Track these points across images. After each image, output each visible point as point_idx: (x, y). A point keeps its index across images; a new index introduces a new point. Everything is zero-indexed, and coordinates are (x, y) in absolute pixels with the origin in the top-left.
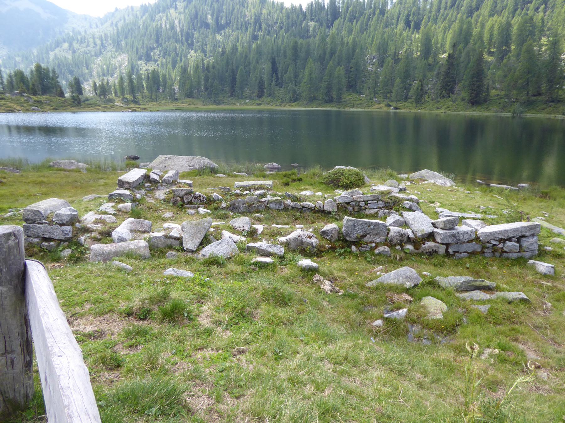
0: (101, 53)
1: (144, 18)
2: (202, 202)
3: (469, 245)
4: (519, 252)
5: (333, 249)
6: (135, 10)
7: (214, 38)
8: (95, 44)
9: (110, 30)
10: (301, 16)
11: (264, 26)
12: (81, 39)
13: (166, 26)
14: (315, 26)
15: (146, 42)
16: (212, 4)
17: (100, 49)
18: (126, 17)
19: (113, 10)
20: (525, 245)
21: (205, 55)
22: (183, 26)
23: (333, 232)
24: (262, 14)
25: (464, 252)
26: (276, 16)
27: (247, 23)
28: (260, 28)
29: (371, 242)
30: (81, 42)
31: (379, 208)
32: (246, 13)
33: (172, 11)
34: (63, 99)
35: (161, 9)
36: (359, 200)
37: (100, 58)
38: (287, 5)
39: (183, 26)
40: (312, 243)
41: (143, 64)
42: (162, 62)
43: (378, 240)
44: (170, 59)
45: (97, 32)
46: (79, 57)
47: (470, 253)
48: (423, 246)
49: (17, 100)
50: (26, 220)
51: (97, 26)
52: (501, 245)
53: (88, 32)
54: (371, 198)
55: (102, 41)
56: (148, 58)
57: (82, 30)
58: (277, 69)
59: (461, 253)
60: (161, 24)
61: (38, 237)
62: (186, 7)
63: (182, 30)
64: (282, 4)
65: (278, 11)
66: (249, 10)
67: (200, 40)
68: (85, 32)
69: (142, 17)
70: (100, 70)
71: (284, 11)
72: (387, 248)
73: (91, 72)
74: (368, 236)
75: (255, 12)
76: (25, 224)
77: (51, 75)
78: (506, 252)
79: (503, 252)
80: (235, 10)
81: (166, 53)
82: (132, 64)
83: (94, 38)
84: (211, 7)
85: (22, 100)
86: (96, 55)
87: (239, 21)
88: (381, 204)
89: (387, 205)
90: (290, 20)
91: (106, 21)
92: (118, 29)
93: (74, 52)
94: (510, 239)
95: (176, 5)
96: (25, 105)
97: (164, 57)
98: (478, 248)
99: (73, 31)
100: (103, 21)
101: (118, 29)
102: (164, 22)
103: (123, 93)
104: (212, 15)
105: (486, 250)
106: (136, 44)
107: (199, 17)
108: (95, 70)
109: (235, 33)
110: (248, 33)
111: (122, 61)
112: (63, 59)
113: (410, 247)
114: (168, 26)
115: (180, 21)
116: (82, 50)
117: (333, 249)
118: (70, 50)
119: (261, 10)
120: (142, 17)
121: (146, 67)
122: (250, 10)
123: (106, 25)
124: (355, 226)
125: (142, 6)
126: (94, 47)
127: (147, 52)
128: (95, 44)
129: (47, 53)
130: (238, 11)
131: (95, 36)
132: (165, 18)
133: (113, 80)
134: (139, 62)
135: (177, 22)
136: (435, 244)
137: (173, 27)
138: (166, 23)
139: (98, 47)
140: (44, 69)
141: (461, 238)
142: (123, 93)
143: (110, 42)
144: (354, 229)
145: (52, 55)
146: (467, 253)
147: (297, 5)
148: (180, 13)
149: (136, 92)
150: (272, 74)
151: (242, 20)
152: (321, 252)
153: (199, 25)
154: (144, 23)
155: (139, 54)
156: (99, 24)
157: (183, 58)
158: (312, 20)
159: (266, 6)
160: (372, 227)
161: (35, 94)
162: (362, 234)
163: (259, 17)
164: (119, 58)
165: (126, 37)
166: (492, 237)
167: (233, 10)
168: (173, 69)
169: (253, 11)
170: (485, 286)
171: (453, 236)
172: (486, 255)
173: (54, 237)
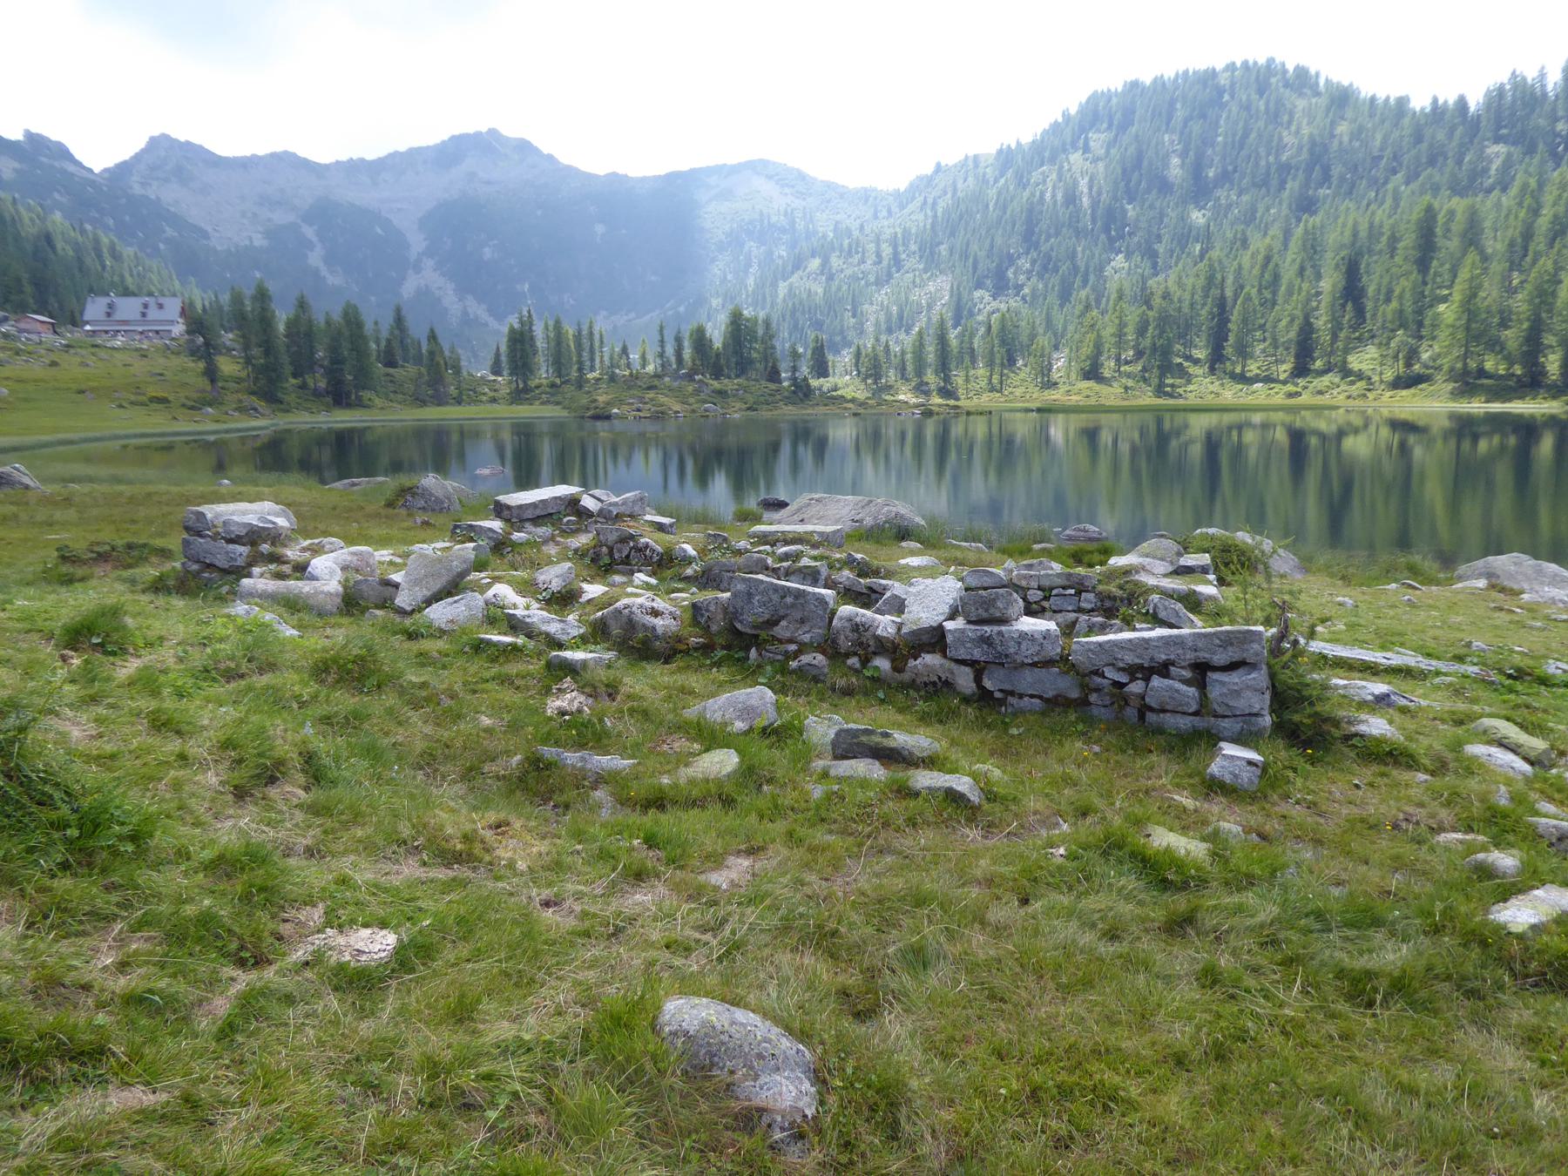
0: (890, 276)
1: (1002, 181)
2: (648, 561)
3: (1040, 673)
4: (1196, 714)
5: (707, 649)
6: (982, 165)
7: (1183, 218)
8: (879, 255)
9: (916, 219)
10: (1460, 130)
11: (1337, 170)
12: (850, 245)
13: (1054, 196)
14: (1509, 155)
15: (999, 241)
16: (1185, 125)
17: (889, 267)
18: (960, 185)
19: (929, 170)
20: (1214, 693)
21: (1154, 266)
22: (1099, 194)
23: (712, 608)
24: (1333, 136)
25: (1032, 696)
26: (1379, 137)
27: (1285, 169)
28: (1326, 178)
29: (791, 641)
30: (850, 251)
31: (1080, 610)
32: (1286, 140)
33: (1076, 158)
34: (773, 386)
35: (1047, 154)
36: (1024, 583)
37: (887, 289)
38: (1420, 102)
39: (1099, 194)
40: (654, 628)
41: (988, 298)
42: (1034, 290)
43: (806, 638)
44: (1055, 280)
45: (888, 227)
46: (839, 289)
47: (1047, 701)
48: (912, 663)
49: (680, 389)
50: (187, 529)
51: (890, 212)
52: (1136, 687)
53: (867, 230)
54: (1059, 582)
55: (895, 247)
56: (1000, 286)
57: (854, 226)
58: (1363, 291)
59: (1021, 696)
60: (1042, 194)
61: (198, 561)
62: (1110, 145)
63: (1095, 205)
64: (1402, 102)
65: (1387, 124)
66: (1293, 128)
67: (1143, 225)
68: (862, 228)
69: (996, 181)
70: (882, 317)
71: (1406, 121)
72: (820, 657)
73: (862, 324)
74: (783, 623)
75: (1311, 135)
76: (185, 536)
77: (760, 332)
78: (1151, 709)
79: (1144, 709)
80: (1253, 135)
81: (1047, 266)
82: (959, 300)
83: (878, 241)
84: (1182, 133)
85: (690, 389)
86: (879, 283)
87: (1263, 163)
88: (1088, 600)
89: (1108, 604)
90: (1424, 146)
91: (913, 198)
92: (935, 216)
93: (831, 278)
94: (1164, 669)
95: (1087, 139)
96: (692, 400)
97: (1041, 276)
98: (1067, 686)
99: (835, 230)
100: (902, 199)
101: (935, 216)
102: (1050, 185)
103: (919, 372)
104: (1183, 155)
105: (1093, 698)
106: (974, 247)
107: (1145, 163)
108: (872, 319)
109: (1245, 198)
110: (1285, 195)
111: (936, 292)
112: (804, 296)
113: (883, 664)
114: (1059, 196)
115: (1091, 180)
116: (849, 272)
117: (707, 649)
118: (822, 273)
119: (1333, 124)
120: (996, 181)
121: (995, 304)
122: (1297, 132)
123: (911, 207)
124: (750, 595)
125: (1000, 152)
126: (875, 264)
127: (999, 266)
128: (879, 255)
129: (774, 285)
130: (1260, 136)
131: (884, 237)
132: (1054, 176)
133: (902, 343)
134: (977, 294)
135: (1083, 184)
136: (943, 661)
137: (1071, 198)
138: (1054, 187)
139: (885, 263)
140: (748, 320)
141: (1012, 650)
142: (919, 372)
143: (913, 247)
144: (749, 601)
145: (783, 288)
146: (1040, 697)
147: (1449, 97)
148: (1096, 160)
149: (953, 366)
150: (1343, 306)
151: (1271, 159)
152: (675, 652)
153: (1143, 185)
154: (999, 194)
155: (979, 272)
156: (895, 209)
157: (1092, 278)
158: (1498, 140)
159: (1349, 114)
160: (789, 600)
161: (717, 375)
162: (767, 617)
163: (1325, 148)
164: (931, 287)
165: (952, 234)
166: (1106, 659)
167: (1246, 135)
168: (1062, 306)
169: (1305, 131)
170: (892, 750)
171: (986, 640)
172: (1095, 711)
173: (217, 563)
